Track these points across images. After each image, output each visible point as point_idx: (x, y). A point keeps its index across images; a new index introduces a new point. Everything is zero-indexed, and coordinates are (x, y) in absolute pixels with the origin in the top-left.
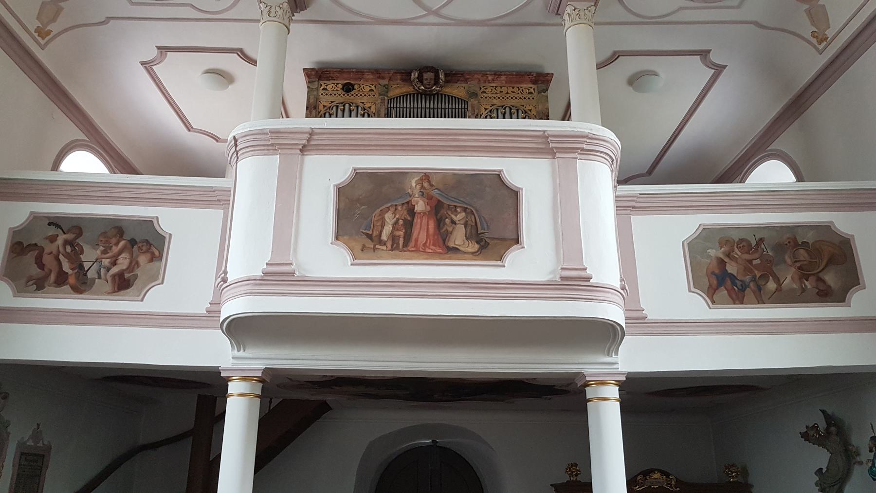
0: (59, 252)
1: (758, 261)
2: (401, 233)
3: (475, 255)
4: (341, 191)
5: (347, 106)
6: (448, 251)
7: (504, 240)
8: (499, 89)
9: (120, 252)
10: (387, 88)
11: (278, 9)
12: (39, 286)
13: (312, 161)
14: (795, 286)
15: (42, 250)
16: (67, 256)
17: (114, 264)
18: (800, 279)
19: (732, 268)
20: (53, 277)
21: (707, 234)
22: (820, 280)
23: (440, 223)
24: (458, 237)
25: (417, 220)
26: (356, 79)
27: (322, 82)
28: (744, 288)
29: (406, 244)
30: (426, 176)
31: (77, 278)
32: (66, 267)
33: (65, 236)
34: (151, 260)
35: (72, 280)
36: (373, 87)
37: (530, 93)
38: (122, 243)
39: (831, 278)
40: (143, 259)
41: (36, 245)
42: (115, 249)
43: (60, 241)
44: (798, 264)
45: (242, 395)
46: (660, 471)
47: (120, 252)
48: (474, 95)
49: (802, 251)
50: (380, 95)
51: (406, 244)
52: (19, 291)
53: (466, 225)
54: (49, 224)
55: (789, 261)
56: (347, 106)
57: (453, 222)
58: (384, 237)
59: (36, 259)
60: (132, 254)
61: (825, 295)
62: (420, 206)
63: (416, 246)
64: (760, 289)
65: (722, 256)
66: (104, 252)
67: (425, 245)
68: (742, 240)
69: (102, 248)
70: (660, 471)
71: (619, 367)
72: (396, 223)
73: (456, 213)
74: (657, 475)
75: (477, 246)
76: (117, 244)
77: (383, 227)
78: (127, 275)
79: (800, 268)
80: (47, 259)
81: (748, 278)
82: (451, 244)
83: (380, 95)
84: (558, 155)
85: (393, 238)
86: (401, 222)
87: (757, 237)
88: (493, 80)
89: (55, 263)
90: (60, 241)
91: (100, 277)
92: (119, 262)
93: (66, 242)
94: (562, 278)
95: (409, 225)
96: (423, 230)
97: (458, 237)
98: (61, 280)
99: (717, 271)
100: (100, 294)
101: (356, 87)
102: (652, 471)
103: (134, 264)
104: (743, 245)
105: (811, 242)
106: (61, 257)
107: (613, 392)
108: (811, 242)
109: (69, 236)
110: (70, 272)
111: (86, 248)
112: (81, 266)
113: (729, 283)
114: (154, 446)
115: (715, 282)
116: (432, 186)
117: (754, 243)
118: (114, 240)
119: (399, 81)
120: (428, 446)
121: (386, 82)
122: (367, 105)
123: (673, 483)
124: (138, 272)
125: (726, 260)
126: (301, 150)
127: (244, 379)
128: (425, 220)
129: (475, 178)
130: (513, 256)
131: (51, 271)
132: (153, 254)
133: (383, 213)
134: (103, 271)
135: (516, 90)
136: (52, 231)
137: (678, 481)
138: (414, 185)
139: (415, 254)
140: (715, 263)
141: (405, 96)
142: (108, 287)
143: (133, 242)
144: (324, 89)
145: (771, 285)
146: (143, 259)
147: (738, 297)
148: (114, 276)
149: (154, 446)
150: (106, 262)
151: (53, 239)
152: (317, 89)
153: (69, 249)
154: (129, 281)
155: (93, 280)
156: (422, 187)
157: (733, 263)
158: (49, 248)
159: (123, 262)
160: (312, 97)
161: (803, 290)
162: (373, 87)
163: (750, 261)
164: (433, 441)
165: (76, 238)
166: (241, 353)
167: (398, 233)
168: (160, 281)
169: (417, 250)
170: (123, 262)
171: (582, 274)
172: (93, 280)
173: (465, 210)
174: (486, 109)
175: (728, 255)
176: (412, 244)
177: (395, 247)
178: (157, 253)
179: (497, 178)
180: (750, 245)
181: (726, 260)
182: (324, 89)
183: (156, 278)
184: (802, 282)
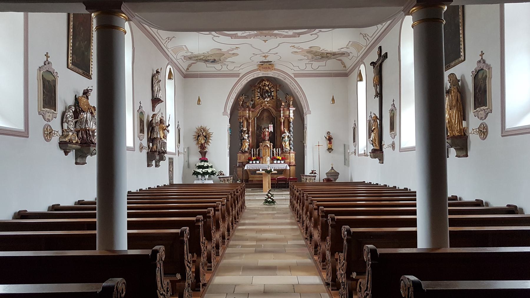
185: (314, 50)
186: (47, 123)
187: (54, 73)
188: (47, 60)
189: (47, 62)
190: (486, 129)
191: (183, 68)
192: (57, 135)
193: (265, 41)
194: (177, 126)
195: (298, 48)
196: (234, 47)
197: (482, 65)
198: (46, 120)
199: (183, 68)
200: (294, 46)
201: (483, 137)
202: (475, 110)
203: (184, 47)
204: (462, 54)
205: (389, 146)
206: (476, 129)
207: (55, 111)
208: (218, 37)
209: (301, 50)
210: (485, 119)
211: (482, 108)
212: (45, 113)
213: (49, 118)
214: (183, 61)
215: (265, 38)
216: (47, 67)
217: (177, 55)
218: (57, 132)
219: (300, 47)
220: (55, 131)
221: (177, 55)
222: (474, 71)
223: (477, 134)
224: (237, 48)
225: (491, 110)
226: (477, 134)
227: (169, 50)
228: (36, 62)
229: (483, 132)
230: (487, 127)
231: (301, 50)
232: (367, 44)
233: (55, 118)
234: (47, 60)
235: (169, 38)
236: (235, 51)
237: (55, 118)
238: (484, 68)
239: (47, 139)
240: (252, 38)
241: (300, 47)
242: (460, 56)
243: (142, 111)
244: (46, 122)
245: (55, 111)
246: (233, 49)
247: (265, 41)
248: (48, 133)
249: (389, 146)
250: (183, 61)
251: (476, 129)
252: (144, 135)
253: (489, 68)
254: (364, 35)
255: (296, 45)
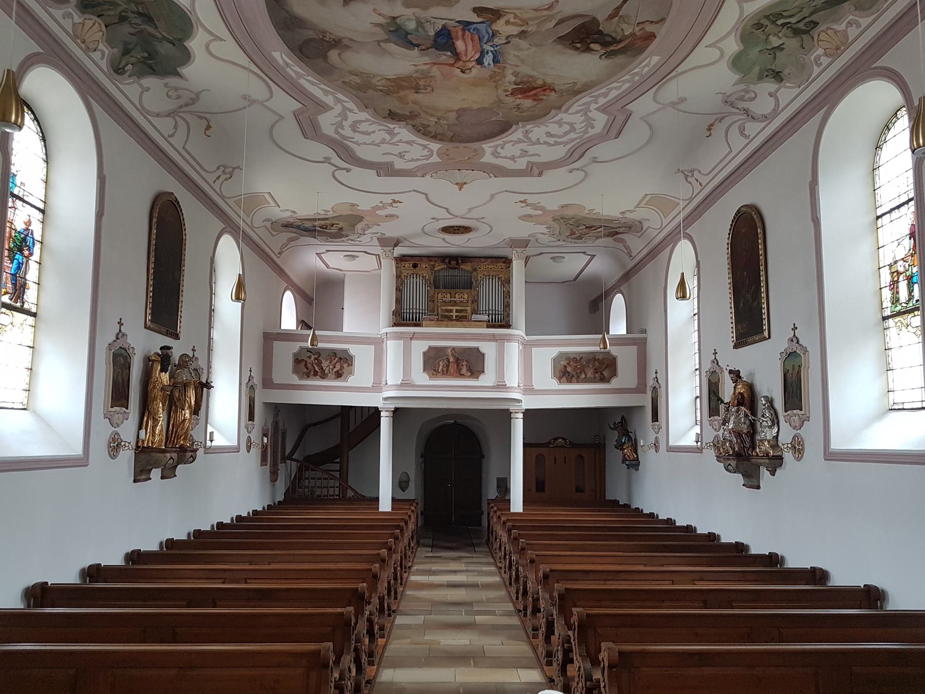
0: (313, 363)
1: (579, 366)
2: (445, 369)
3: (469, 377)
4: (424, 354)
5: (415, 275)
6: (461, 376)
7: (479, 371)
8: (487, 266)
9: (337, 362)
10: (434, 266)
11: (389, 253)
12: (308, 376)
13: (414, 343)
14: (592, 376)
15: (306, 362)
16: (316, 364)
17: (335, 367)
18: (594, 373)
19: (569, 369)
20: (312, 373)
21: (561, 355)
22: (602, 374)
23: (458, 365)
24: (464, 371)
25: (450, 364)
26: (419, 261)
27: (402, 263)
28: (573, 376)
29: (447, 373)
30: (453, 349)
31: (322, 373)
32: (317, 369)
33: (314, 356)
34: (348, 366)
35: (319, 374)
36: (427, 266)
37: (502, 268)
38: (336, 359)
39: (605, 373)
40: (345, 366)
41: (303, 360)
42: (335, 362)
43: (313, 358)
44: (594, 368)
45: (387, 417)
46: (562, 438)
47: (337, 362)
48: (475, 270)
49: (596, 362)
50: (430, 270)
51: (447, 373)
52: (301, 378)
53: (467, 366)
54: (308, 351)
55: (591, 366)
56: (415, 275)
57: (462, 365)
58: (440, 371)
59: (305, 365)
60: (341, 363)
61: (603, 380)
62: (451, 360)
63: (450, 373)
64: (578, 377)
65: (565, 364)
66: (330, 363)
67: (453, 373)
68: (574, 358)
69: (329, 361)
70: (562, 438)
71: (523, 405)
72: (444, 365)
73: (463, 362)
74: (561, 440)
75: (470, 374)
76: (335, 359)
77: (439, 366)
78: (340, 372)
79: (595, 369)
80: (309, 365)
81: (574, 373)
82: (462, 373)
83: (430, 270)
84: (499, 341)
85: (443, 370)
86: (445, 365)
87: (581, 356)
88: (484, 262)
89: (312, 367)
90: (313, 358)
91: (330, 373)
92: (336, 366)
93: (315, 359)
94: (497, 385)
95: (448, 366)
96: (453, 367)
97: (464, 371)
98: (316, 374)
99: (563, 370)
100: (331, 379)
101: (419, 265)
102: (558, 438)
103: (342, 368)
104: (575, 360)
105: (601, 359)
106: (314, 365)
107: (521, 415)
108: (601, 359)
109: (316, 356)
110: (318, 370)
111: (323, 361)
112: (322, 368)
113: (567, 374)
114: (315, 424)
115: (562, 375)
116: (455, 352)
117: (579, 359)
118: (333, 358)
119: (439, 262)
120: (453, 424)
121: (433, 263)
122: (425, 275)
123: (568, 443)
124: (344, 370)
125: (567, 366)
126: (411, 339)
127: (386, 411)
128: (453, 365)
129: (470, 349)
130: (482, 377)
131: (311, 370)
132: (349, 363)
133: (439, 362)
134: (331, 370)
135: (495, 266)
136: (309, 354)
137: (570, 442)
138: (449, 351)
139: (450, 377)
140: (562, 367)
141: (442, 269)
142: (334, 377)
143: (340, 359)
144: (404, 267)
145: (583, 376)
146: (345, 366)
147: (570, 381)
148: (335, 372)
149: (315, 424)
150: (331, 367)
151: (310, 357)
152: (400, 267)
153: (316, 361)
154: (340, 374)
155: (328, 374)
156: (452, 353)
157: (570, 367)
158: (309, 361)
159: (338, 367)
160: (398, 271)
161: (595, 378)
162: (427, 266)
163: (576, 366)
164: (455, 421)
165: (318, 357)
166: (386, 402)
167: (444, 369)
168: (353, 374)
169: (450, 375)
170: (338, 367)
171: (503, 383)
172: (328, 374)
173: (466, 361)
174: (480, 277)
175: (568, 364)
176: (449, 373)
177: (443, 374)
178: (350, 363)
179: (478, 349)
180: (577, 360)
181: (567, 366)
182: (404, 267)
183: (351, 373)
184: (594, 374)
185: (569, 213)
186: (115, 429)
187: (129, 350)
188: (120, 331)
189: (121, 334)
190: (801, 445)
191: (260, 238)
192: (129, 449)
193: (461, 186)
194: (245, 380)
195: (535, 207)
196: (388, 199)
197: (795, 347)
198: (114, 425)
199: (260, 238)
200: (524, 202)
201: (797, 456)
202: (786, 414)
203: (266, 196)
204: (765, 327)
205: (708, 445)
206: (788, 444)
207: (127, 409)
208: (348, 170)
209: (540, 212)
210: (800, 429)
211: (795, 411)
212: (113, 414)
213: (118, 422)
214: (272, 235)
215: (459, 176)
216: (120, 343)
217: (252, 218)
218: (129, 443)
219: (540, 204)
220: (125, 442)
221: (252, 218)
222: (783, 353)
223: (788, 452)
224: (394, 201)
225: (809, 417)
226: (788, 452)
227: (231, 202)
228: (107, 337)
229: (798, 448)
230: (803, 443)
231: (540, 212)
232: (694, 194)
233: (127, 419)
234: (120, 331)
235: (225, 167)
236: (390, 211)
237: (127, 419)
238: (797, 351)
239: (113, 454)
240: (428, 177)
241: (540, 204)
242: (762, 331)
243: (198, 368)
244: (113, 429)
245: (127, 409)
246: (384, 207)
247: (461, 186)
248: (115, 445)
249: (708, 445)
250: (272, 235)
251: (788, 444)
252: (198, 418)
253: (805, 350)
254: (686, 173)
255: (531, 199)
